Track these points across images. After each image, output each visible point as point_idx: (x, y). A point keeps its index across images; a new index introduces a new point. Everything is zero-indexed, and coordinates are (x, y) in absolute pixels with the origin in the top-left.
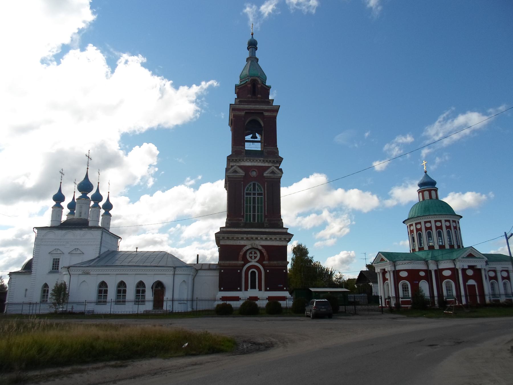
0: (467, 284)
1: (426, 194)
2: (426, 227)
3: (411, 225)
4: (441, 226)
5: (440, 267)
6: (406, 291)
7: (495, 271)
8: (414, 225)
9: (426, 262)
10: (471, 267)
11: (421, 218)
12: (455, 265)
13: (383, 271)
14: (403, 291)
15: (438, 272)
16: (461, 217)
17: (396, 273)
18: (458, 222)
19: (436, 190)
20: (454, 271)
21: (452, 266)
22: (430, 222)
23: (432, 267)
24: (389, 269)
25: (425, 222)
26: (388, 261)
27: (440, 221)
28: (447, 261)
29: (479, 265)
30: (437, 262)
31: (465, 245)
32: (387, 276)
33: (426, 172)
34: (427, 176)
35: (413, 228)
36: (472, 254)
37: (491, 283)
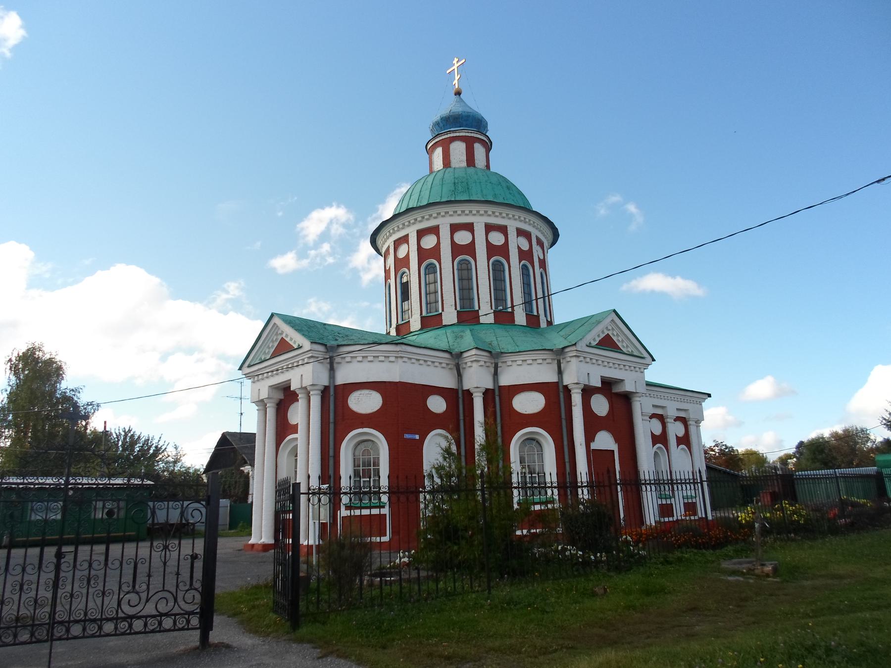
0: (594, 446)
1: (458, 150)
2: (489, 244)
3: (405, 239)
5: (506, 380)
9: (456, 359)
10: (608, 386)
12: (560, 372)
13: (280, 395)
17: (335, 397)
19: (488, 146)
20: (556, 393)
21: (548, 375)
22: (469, 227)
23: (477, 379)
24: (307, 382)
25: (455, 228)
27: (503, 230)
28: (540, 356)
32: (296, 414)
33: (458, 93)
35: (410, 250)
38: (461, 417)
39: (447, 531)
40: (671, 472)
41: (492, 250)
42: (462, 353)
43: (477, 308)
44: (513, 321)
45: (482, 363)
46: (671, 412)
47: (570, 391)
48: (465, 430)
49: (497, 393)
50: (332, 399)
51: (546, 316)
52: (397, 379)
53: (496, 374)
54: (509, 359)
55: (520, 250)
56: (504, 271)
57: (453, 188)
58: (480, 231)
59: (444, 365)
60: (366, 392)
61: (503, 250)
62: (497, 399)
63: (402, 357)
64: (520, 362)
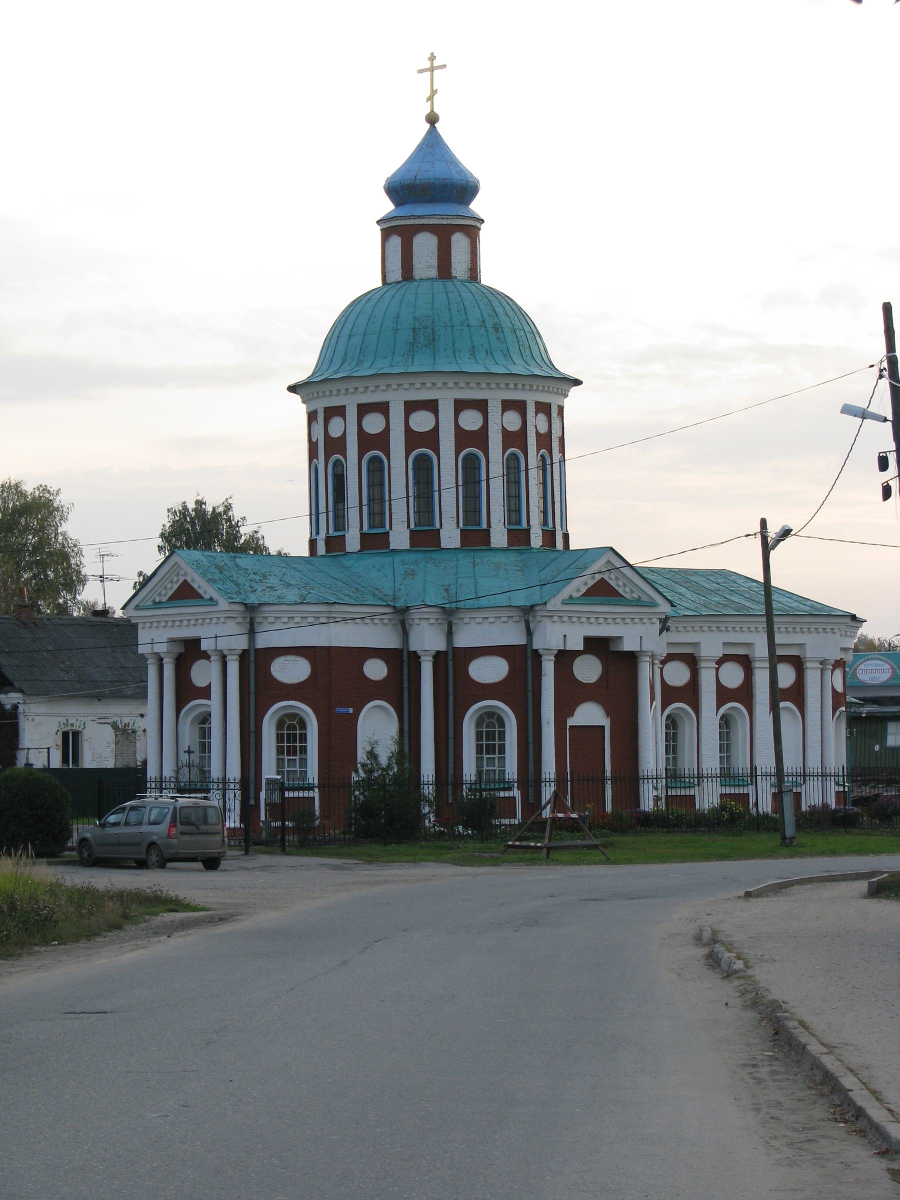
0: (571, 722)
1: (425, 246)
2: (408, 431)
3: (340, 411)
4: (436, 428)
5: (463, 640)
6: (292, 751)
7: (692, 661)
8: (352, 414)
9: (402, 617)
11: (394, 382)
12: (529, 634)
13: (180, 649)
14: (280, 751)
15: (453, 662)
16: (577, 382)
17: (256, 663)
18: (561, 409)
19: (472, 230)
20: (523, 660)
21: (513, 636)
22: (432, 406)
23: (428, 639)
24: (223, 644)
26: (223, 605)
28: (504, 614)
29: (635, 634)
30: (449, 616)
34: (432, 144)
36: (609, 582)
37: (418, 459)
38: (406, 685)
39: (366, 810)
40: (208, 833)
41: (463, 438)
43: (438, 526)
44: (488, 542)
47: (540, 656)
48: (409, 700)
49: (450, 657)
50: (252, 666)
51: (545, 523)
53: (450, 634)
54: (467, 616)
56: (479, 468)
57: (411, 339)
59: (386, 621)
61: (480, 438)
62: (450, 663)
64: (480, 620)
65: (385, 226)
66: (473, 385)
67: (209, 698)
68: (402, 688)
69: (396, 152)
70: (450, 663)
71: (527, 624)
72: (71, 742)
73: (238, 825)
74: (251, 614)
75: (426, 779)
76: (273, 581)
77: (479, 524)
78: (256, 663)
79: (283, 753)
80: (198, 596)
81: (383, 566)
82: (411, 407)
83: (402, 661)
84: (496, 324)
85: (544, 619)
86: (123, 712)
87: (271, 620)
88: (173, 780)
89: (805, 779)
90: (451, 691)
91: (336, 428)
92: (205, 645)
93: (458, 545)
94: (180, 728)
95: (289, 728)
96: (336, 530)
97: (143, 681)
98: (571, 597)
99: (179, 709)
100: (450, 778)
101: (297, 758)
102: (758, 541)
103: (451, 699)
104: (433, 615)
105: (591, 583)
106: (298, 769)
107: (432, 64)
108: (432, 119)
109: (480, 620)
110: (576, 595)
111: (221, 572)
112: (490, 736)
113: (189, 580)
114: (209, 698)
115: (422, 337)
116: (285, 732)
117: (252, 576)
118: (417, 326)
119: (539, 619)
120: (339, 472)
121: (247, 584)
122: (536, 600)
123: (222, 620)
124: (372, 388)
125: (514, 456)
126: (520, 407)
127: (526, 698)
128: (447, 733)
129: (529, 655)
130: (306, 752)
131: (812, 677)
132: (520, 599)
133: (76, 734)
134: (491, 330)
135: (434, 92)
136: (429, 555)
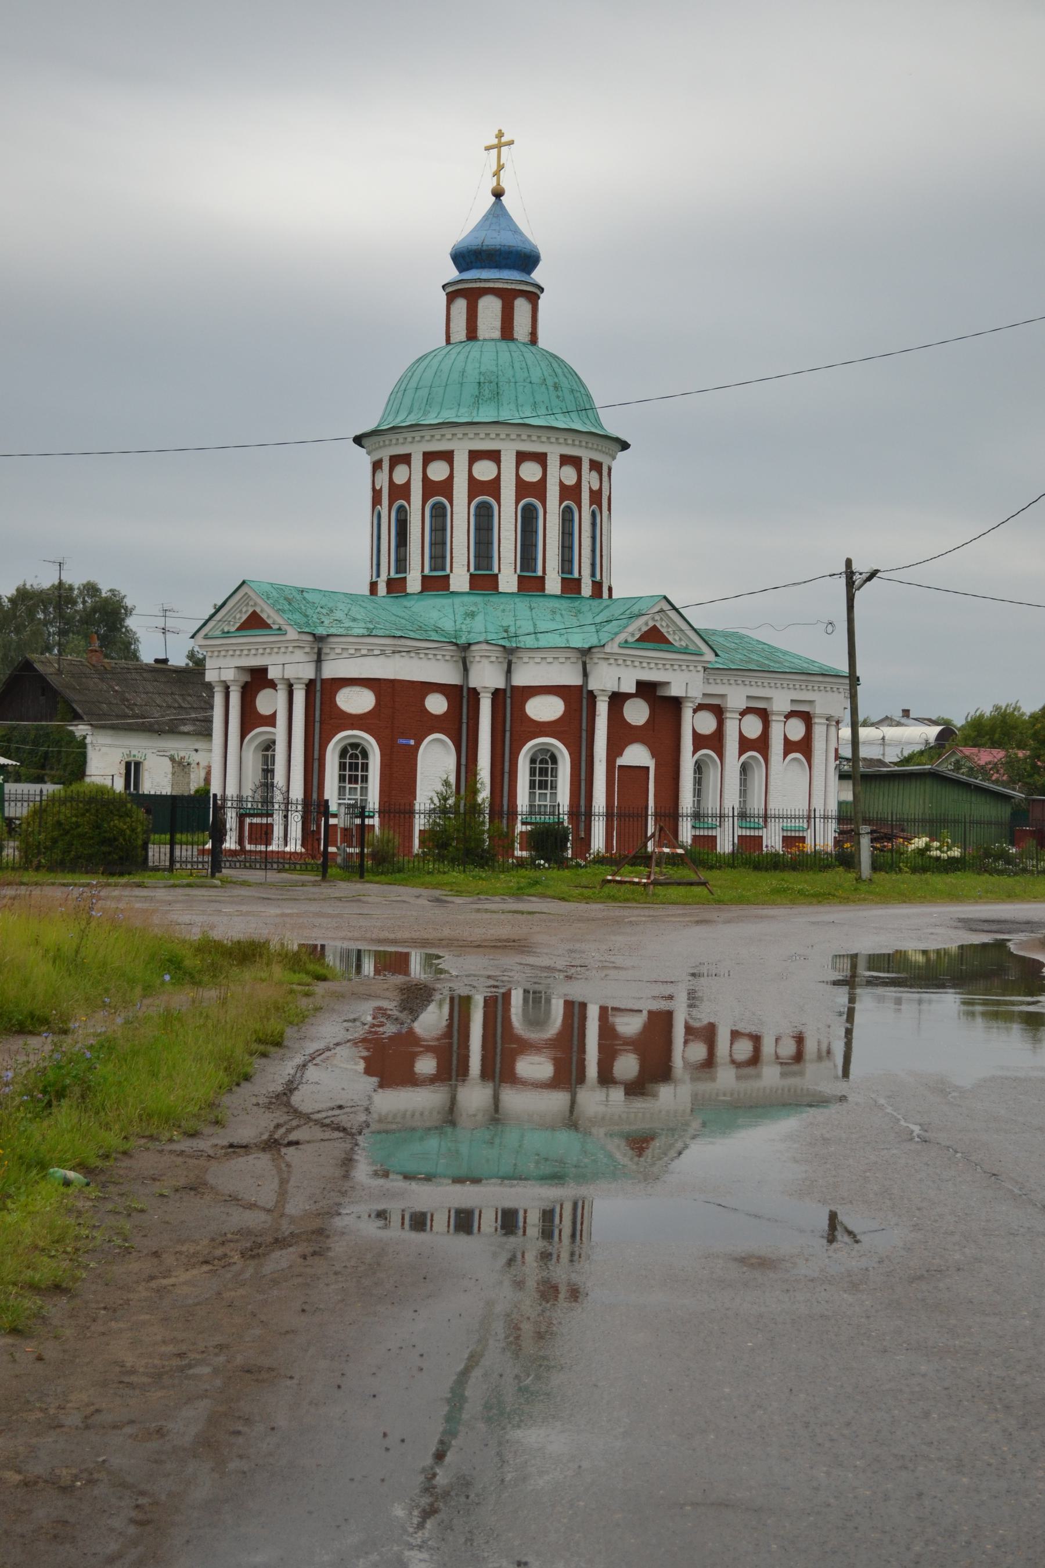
0: (621, 761)
1: (490, 309)
2: (471, 478)
4: (497, 479)
6: (354, 779)
8: (417, 462)
9: (463, 652)
10: (647, 690)
12: (585, 675)
14: (342, 778)
15: (510, 700)
16: (625, 446)
17: (321, 693)
19: (533, 296)
21: (571, 677)
22: (494, 456)
23: (487, 677)
24: (290, 673)
26: (292, 634)
27: (541, 459)
28: (562, 655)
29: (682, 682)
30: (509, 656)
31: (624, 584)
37: (479, 507)
38: (465, 720)
41: (523, 488)
42: (470, 644)
43: (496, 571)
44: (543, 589)
45: (493, 659)
46: (781, 702)
47: (595, 697)
48: (468, 735)
49: (508, 694)
50: (318, 695)
51: (593, 575)
52: (392, 677)
53: (509, 672)
54: (526, 656)
55: (562, 486)
58: (508, 461)
59: (447, 658)
60: (357, 689)
61: (538, 489)
62: (508, 701)
63: (400, 652)
64: (539, 660)
65: (450, 289)
66: (534, 438)
67: (274, 726)
68: (461, 723)
69: (462, 220)
70: (508, 701)
71: (584, 664)
72: (133, 770)
73: (299, 849)
74: (319, 645)
75: (685, 811)
76: (339, 615)
77: (535, 571)
78: (321, 693)
79: (344, 781)
80: (267, 626)
81: (443, 607)
82: (475, 456)
83: (462, 698)
84: (555, 383)
85: (601, 662)
86: (181, 747)
87: (338, 651)
88: (250, 799)
89: (766, 822)
90: (508, 728)
91: (400, 475)
92: (271, 675)
93: (515, 589)
94: (243, 753)
95: (351, 757)
96: (397, 572)
97: (205, 709)
98: (626, 642)
99: (243, 737)
100: (505, 808)
101: (358, 786)
102: (843, 580)
103: (508, 734)
104: (495, 654)
105: (645, 629)
106: (358, 797)
107: (500, 141)
108: (498, 194)
109: (539, 660)
110: (631, 639)
111: (290, 604)
112: (543, 772)
113: (258, 610)
114: (274, 726)
115: (487, 391)
116: (348, 761)
117: (319, 609)
118: (482, 380)
119: (596, 660)
120: (403, 518)
121: (315, 616)
122: (593, 641)
123: (290, 649)
124: (438, 437)
125: (568, 507)
126: (575, 462)
127: (580, 737)
128: (503, 768)
129: (585, 695)
130: (367, 781)
131: (819, 731)
132: (578, 641)
133: (138, 765)
134: (551, 388)
135: (501, 167)
136: (487, 598)
